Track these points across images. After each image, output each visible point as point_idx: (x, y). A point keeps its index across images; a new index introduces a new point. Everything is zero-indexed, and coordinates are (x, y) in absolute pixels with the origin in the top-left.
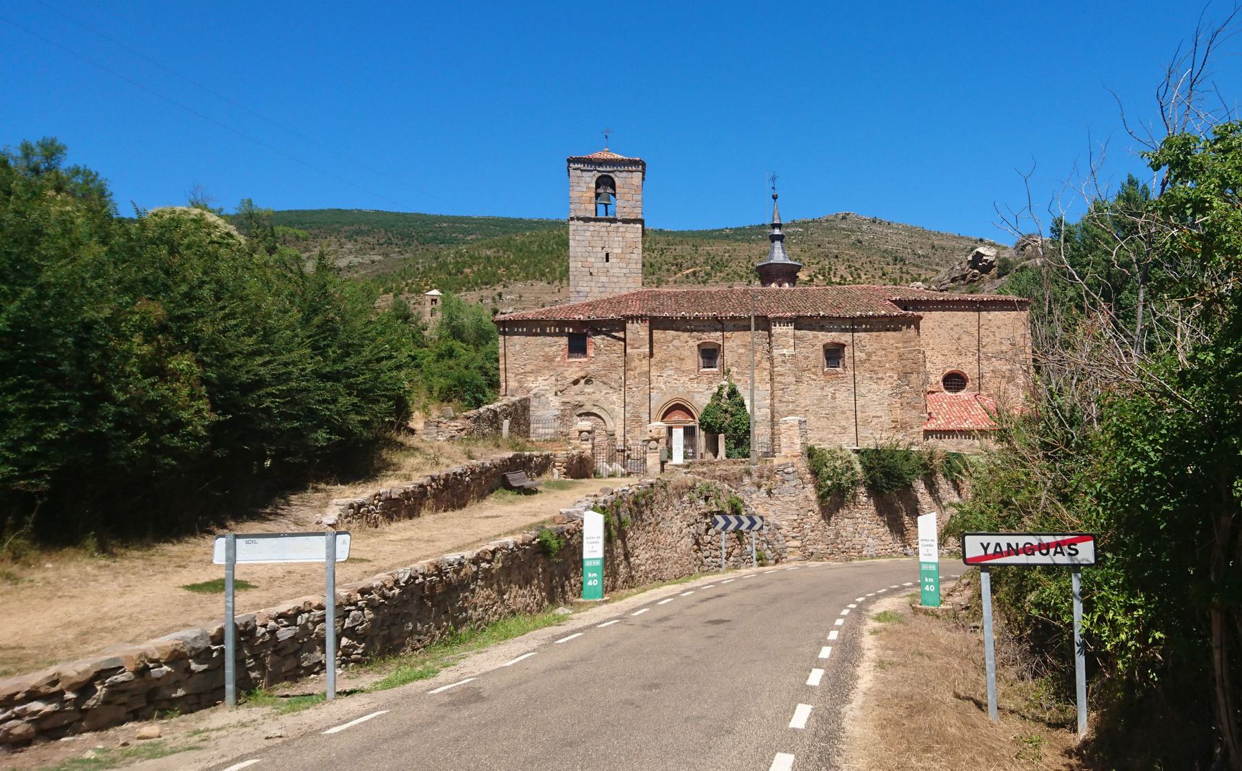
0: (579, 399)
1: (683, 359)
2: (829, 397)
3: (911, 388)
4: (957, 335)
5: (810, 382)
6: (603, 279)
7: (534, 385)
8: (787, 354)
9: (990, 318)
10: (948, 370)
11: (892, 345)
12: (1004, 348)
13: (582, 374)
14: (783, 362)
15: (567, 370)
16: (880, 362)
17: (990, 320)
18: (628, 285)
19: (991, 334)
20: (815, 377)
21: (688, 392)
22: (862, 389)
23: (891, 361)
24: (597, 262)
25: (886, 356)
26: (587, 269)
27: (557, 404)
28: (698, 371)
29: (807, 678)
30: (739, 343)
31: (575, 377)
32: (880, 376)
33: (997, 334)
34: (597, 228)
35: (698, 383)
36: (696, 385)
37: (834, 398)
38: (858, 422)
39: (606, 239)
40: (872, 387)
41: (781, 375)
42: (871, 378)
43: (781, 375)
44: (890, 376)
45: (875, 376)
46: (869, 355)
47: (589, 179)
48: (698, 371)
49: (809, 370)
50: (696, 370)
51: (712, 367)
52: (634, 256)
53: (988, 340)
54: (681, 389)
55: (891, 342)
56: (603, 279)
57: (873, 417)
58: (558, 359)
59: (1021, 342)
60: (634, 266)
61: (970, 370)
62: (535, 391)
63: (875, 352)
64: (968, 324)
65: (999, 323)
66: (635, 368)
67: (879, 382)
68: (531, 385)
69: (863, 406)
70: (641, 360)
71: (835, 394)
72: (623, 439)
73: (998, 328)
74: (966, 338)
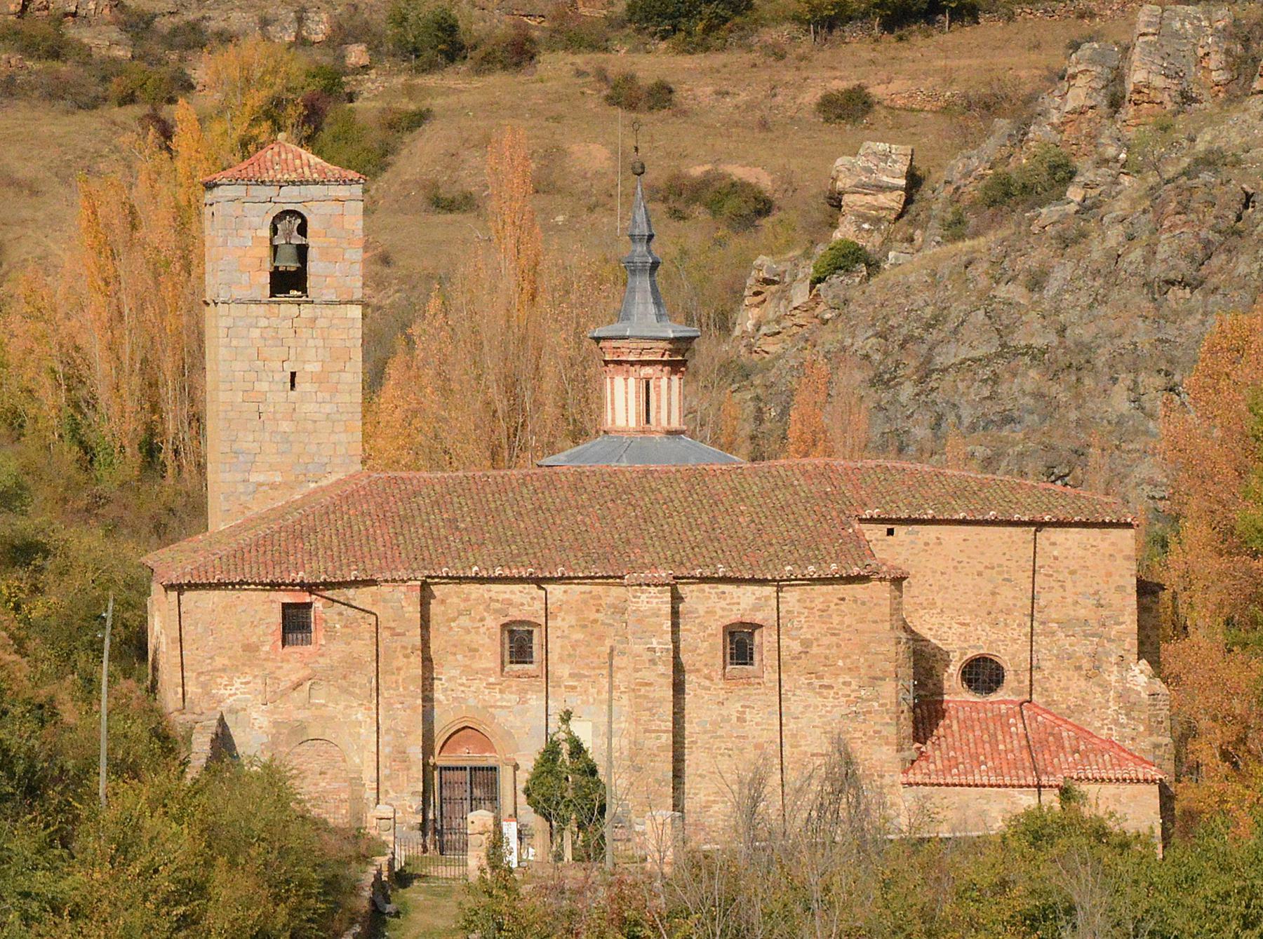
0: (300, 717)
1: (476, 650)
2: (734, 719)
3: (882, 705)
4: (990, 587)
5: (698, 691)
6: (285, 426)
7: (228, 692)
8: (658, 647)
9: (1056, 553)
10: (971, 654)
11: (849, 626)
12: (1082, 613)
13: (307, 672)
14: (653, 662)
15: (280, 668)
16: (826, 658)
17: (1056, 558)
18: (334, 438)
19: (1056, 585)
20: (707, 683)
21: (485, 707)
22: (793, 705)
23: (846, 657)
24: (272, 387)
25: (838, 646)
26: (254, 406)
27: (266, 724)
28: (502, 670)
29: (171, 101)
30: (573, 623)
31: (295, 678)
32: (826, 682)
33: (1069, 585)
34: (274, 322)
35: (501, 692)
36: (498, 696)
37: (741, 720)
38: (785, 764)
39: (291, 342)
40: (810, 701)
41: (647, 684)
42: (809, 684)
43: (647, 684)
44: (844, 683)
45: (817, 683)
46: (806, 644)
47: (256, 221)
48: (502, 670)
49: (698, 670)
50: (498, 669)
51: (525, 662)
52: (347, 377)
53: (1050, 596)
54: (472, 702)
55: (847, 620)
56: (285, 426)
57: (813, 755)
58: (266, 648)
59: (1116, 599)
60: (347, 398)
61: (1010, 655)
62: (230, 701)
63: (817, 639)
64: (1013, 564)
65: (1074, 565)
66: (399, 669)
67: (825, 692)
68: (222, 691)
69: (794, 736)
70: (406, 656)
71: (744, 712)
72: (375, 785)
73: (1073, 573)
74: (1007, 593)
